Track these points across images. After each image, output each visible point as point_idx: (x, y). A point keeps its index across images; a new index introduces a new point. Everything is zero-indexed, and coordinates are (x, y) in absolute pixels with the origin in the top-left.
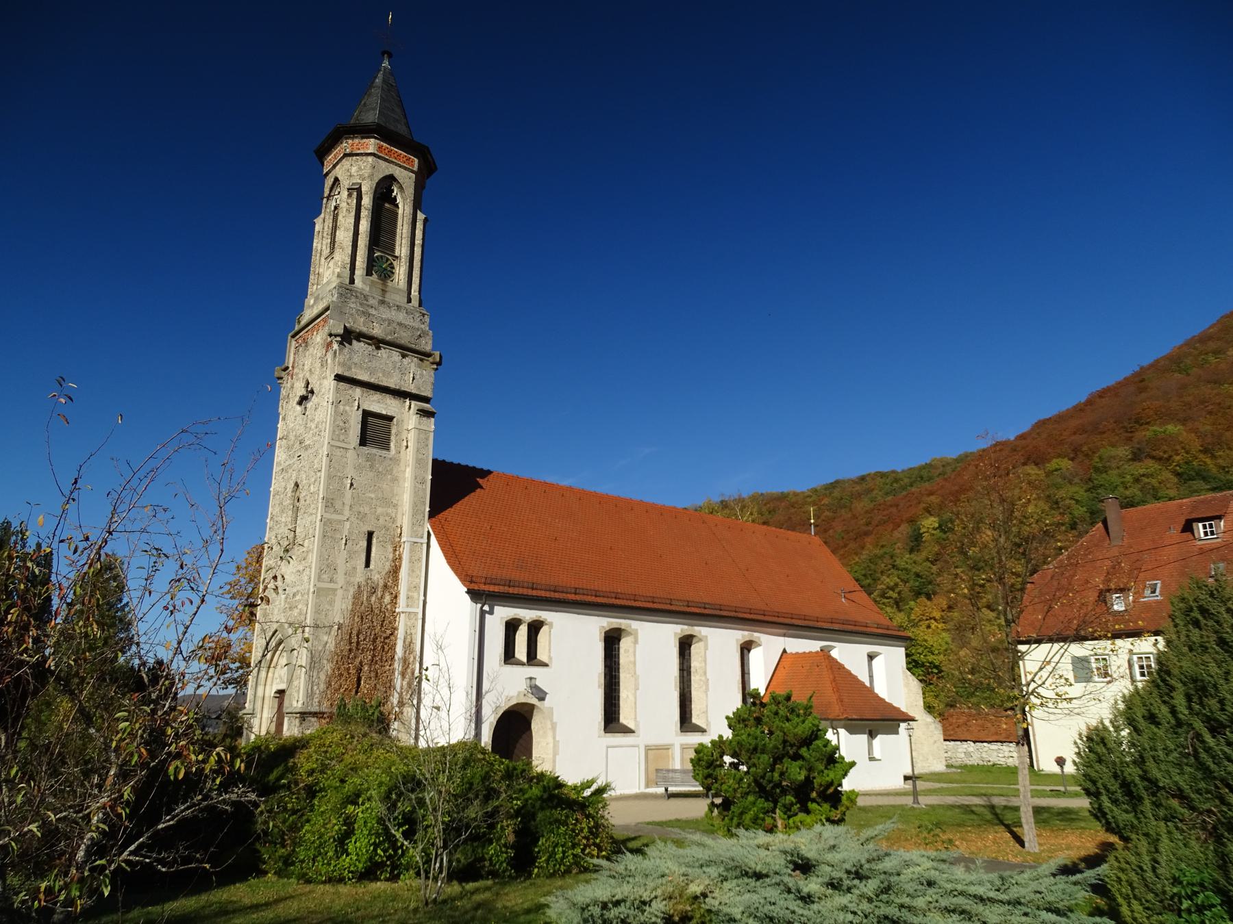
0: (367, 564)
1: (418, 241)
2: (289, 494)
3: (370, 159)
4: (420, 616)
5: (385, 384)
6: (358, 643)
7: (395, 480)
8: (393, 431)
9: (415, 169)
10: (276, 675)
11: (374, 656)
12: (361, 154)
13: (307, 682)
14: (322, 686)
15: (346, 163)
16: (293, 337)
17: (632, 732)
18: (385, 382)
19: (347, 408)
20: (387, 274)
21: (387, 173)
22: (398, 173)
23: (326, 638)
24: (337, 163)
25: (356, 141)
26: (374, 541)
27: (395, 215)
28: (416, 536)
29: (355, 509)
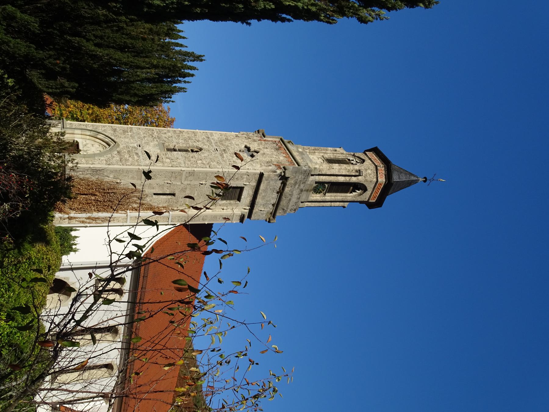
0: (155, 194)
2: (195, 144)
3: (375, 180)
4: (125, 224)
5: (258, 197)
6: (109, 193)
8: (232, 202)
9: (370, 201)
10: (88, 142)
11: (100, 202)
12: (377, 175)
13: (84, 168)
14: (82, 176)
15: (373, 167)
16: (281, 139)
18: (259, 197)
19: (245, 179)
20: (316, 190)
22: (368, 193)
24: (372, 161)
25: (384, 172)
26: (170, 197)
27: (346, 192)
28: (172, 219)
29: (188, 187)
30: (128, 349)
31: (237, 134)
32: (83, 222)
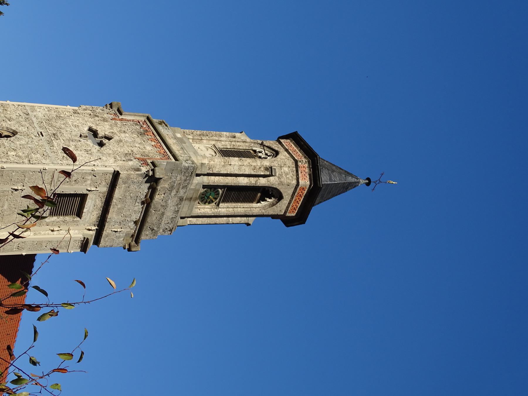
3: (294, 182)
8: (68, 218)
15: (290, 162)
16: (148, 118)
19: (89, 182)
20: (204, 199)
21: (284, 195)
22: (284, 203)
24: (289, 153)
25: (307, 170)
27: (252, 201)
31: (76, 108)
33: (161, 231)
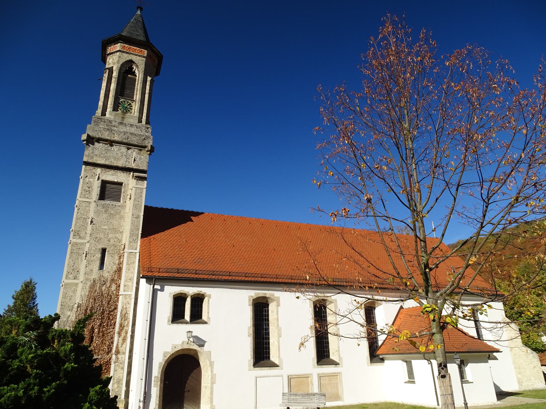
1: (147, 91)
5: (115, 164)
7: (122, 217)
17: (278, 366)
18: (115, 164)
19: (91, 180)
21: (128, 59)
23: (69, 313)
25: (112, 47)
29: (94, 236)
30: (341, 287)
32: (124, 340)
33: (147, 134)
